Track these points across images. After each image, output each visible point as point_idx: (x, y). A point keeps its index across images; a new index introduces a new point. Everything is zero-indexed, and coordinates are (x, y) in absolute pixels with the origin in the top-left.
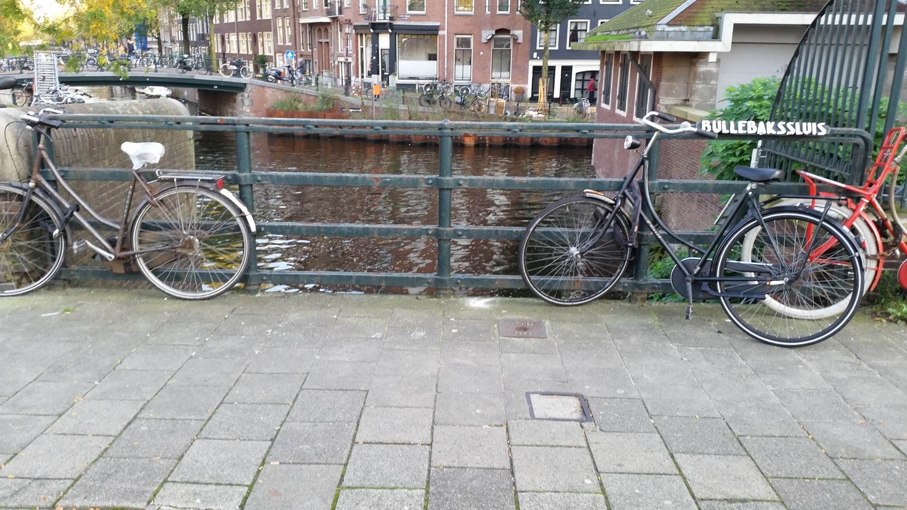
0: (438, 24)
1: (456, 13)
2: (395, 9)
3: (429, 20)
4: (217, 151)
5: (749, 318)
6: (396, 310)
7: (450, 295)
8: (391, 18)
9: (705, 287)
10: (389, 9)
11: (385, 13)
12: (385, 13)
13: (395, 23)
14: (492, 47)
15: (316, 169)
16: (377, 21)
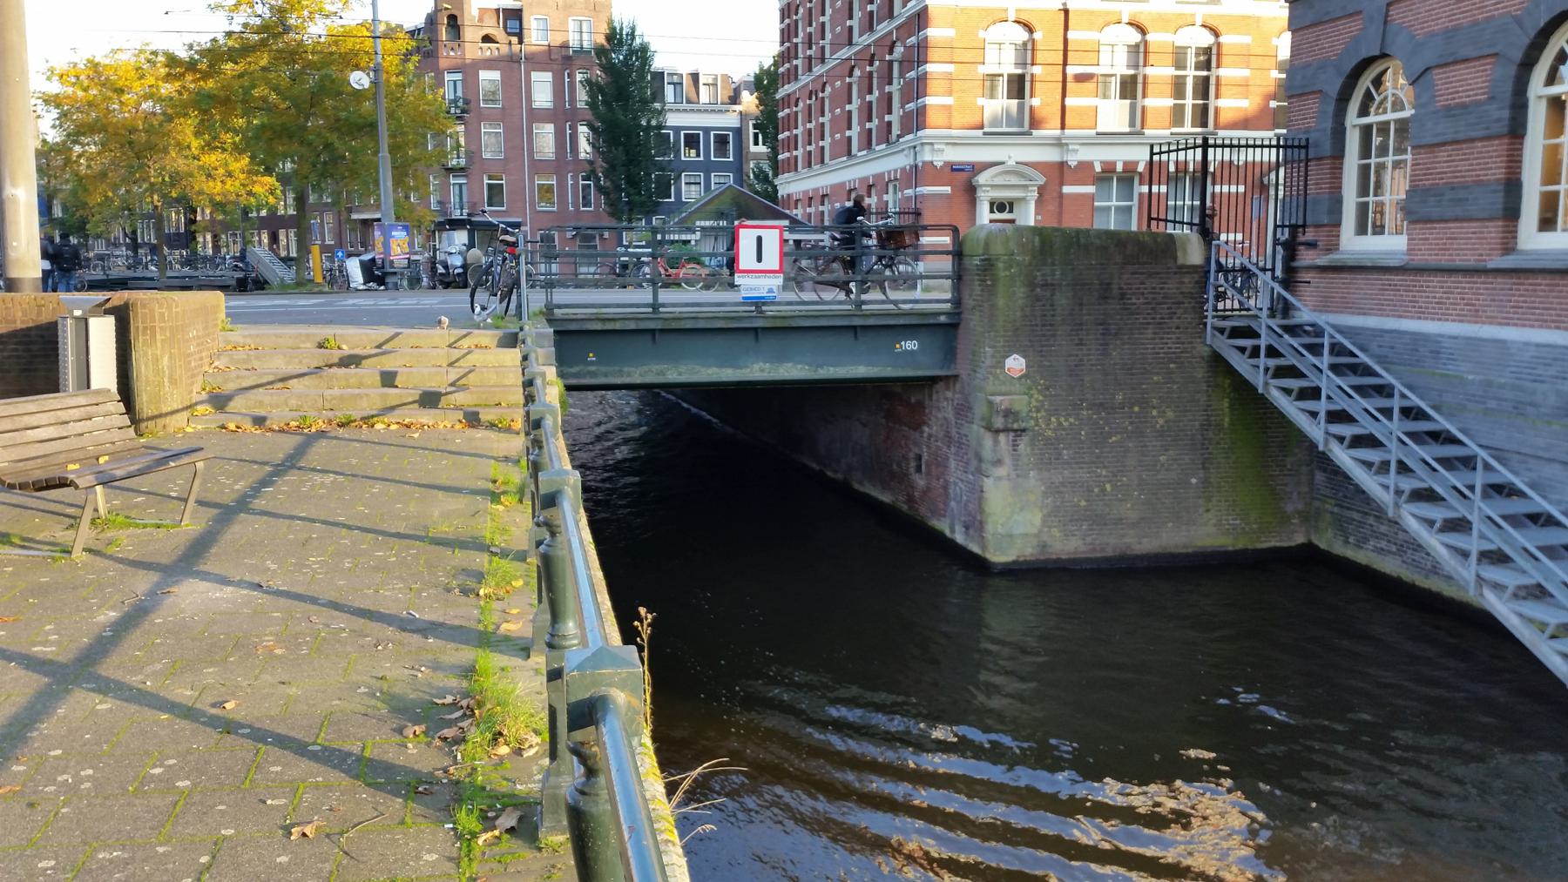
0: (520, 220)
1: (538, 209)
2: (473, 205)
3: (510, 216)
4: (1068, 769)
5: (236, 160)
6: (1212, 874)
7: (776, 64)
8: (469, 215)
9: (64, 77)
10: (466, 206)
11: (462, 209)
12: (462, 209)
13: (473, 219)
14: (578, 243)
15: (1476, 316)
16: (453, 217)
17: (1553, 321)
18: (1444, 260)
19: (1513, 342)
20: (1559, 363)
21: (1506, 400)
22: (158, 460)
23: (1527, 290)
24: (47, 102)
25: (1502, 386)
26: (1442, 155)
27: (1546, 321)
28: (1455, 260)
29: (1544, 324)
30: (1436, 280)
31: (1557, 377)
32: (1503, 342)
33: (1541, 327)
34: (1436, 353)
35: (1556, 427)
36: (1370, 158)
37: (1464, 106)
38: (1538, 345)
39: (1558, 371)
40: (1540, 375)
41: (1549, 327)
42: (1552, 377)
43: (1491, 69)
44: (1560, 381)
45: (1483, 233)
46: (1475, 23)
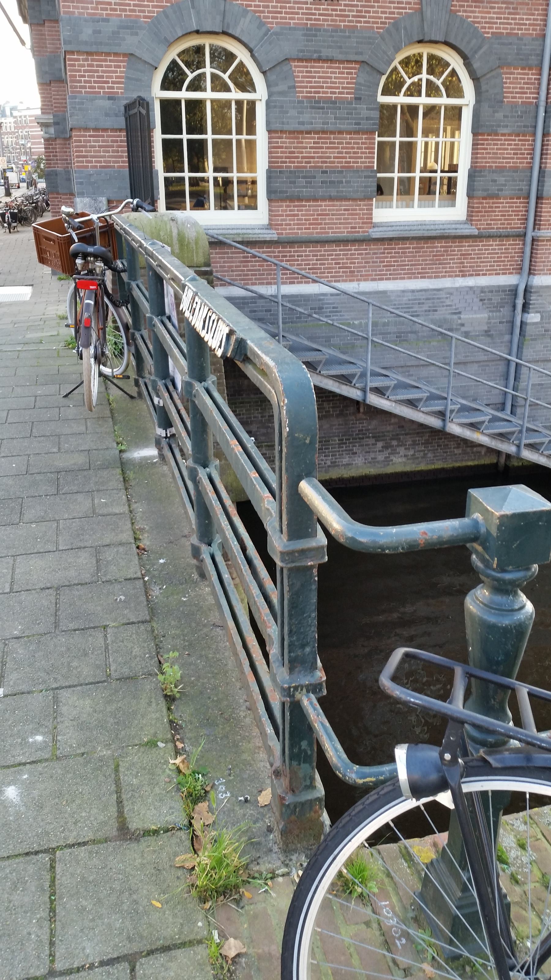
17: (418, 273)
18: (315, 233)
19: (392, 292)
20: (430, 301)
21: (390, 333)
22: (182, 456)
23: (398, 253)
24: (371, 845)
25: (385, 324)
26: (309, 142)
27: (414, 273)
28: (328, 233)
29: (412, 275)
30: (308, 250)
31: (429, 311)
32: (384, 292)
33: (410, 278)
34: (320, 310)
35: (434, 343)
36: (181, 141)
37: (329, 101)
38: (413, 291)
39: (429, 307)
40: (416, 311)
41: (417, 278)
42: (426, 311)
43: (355, 73)
44: (431, 313)
45: (356, 210)
46: (336, 29)
